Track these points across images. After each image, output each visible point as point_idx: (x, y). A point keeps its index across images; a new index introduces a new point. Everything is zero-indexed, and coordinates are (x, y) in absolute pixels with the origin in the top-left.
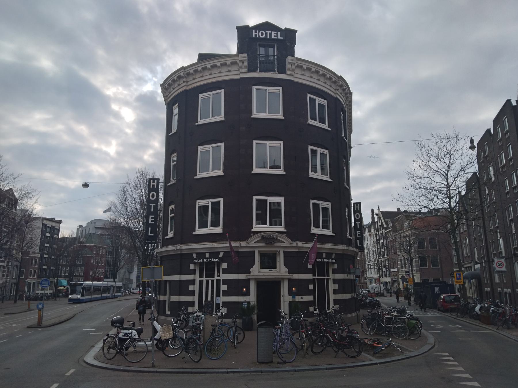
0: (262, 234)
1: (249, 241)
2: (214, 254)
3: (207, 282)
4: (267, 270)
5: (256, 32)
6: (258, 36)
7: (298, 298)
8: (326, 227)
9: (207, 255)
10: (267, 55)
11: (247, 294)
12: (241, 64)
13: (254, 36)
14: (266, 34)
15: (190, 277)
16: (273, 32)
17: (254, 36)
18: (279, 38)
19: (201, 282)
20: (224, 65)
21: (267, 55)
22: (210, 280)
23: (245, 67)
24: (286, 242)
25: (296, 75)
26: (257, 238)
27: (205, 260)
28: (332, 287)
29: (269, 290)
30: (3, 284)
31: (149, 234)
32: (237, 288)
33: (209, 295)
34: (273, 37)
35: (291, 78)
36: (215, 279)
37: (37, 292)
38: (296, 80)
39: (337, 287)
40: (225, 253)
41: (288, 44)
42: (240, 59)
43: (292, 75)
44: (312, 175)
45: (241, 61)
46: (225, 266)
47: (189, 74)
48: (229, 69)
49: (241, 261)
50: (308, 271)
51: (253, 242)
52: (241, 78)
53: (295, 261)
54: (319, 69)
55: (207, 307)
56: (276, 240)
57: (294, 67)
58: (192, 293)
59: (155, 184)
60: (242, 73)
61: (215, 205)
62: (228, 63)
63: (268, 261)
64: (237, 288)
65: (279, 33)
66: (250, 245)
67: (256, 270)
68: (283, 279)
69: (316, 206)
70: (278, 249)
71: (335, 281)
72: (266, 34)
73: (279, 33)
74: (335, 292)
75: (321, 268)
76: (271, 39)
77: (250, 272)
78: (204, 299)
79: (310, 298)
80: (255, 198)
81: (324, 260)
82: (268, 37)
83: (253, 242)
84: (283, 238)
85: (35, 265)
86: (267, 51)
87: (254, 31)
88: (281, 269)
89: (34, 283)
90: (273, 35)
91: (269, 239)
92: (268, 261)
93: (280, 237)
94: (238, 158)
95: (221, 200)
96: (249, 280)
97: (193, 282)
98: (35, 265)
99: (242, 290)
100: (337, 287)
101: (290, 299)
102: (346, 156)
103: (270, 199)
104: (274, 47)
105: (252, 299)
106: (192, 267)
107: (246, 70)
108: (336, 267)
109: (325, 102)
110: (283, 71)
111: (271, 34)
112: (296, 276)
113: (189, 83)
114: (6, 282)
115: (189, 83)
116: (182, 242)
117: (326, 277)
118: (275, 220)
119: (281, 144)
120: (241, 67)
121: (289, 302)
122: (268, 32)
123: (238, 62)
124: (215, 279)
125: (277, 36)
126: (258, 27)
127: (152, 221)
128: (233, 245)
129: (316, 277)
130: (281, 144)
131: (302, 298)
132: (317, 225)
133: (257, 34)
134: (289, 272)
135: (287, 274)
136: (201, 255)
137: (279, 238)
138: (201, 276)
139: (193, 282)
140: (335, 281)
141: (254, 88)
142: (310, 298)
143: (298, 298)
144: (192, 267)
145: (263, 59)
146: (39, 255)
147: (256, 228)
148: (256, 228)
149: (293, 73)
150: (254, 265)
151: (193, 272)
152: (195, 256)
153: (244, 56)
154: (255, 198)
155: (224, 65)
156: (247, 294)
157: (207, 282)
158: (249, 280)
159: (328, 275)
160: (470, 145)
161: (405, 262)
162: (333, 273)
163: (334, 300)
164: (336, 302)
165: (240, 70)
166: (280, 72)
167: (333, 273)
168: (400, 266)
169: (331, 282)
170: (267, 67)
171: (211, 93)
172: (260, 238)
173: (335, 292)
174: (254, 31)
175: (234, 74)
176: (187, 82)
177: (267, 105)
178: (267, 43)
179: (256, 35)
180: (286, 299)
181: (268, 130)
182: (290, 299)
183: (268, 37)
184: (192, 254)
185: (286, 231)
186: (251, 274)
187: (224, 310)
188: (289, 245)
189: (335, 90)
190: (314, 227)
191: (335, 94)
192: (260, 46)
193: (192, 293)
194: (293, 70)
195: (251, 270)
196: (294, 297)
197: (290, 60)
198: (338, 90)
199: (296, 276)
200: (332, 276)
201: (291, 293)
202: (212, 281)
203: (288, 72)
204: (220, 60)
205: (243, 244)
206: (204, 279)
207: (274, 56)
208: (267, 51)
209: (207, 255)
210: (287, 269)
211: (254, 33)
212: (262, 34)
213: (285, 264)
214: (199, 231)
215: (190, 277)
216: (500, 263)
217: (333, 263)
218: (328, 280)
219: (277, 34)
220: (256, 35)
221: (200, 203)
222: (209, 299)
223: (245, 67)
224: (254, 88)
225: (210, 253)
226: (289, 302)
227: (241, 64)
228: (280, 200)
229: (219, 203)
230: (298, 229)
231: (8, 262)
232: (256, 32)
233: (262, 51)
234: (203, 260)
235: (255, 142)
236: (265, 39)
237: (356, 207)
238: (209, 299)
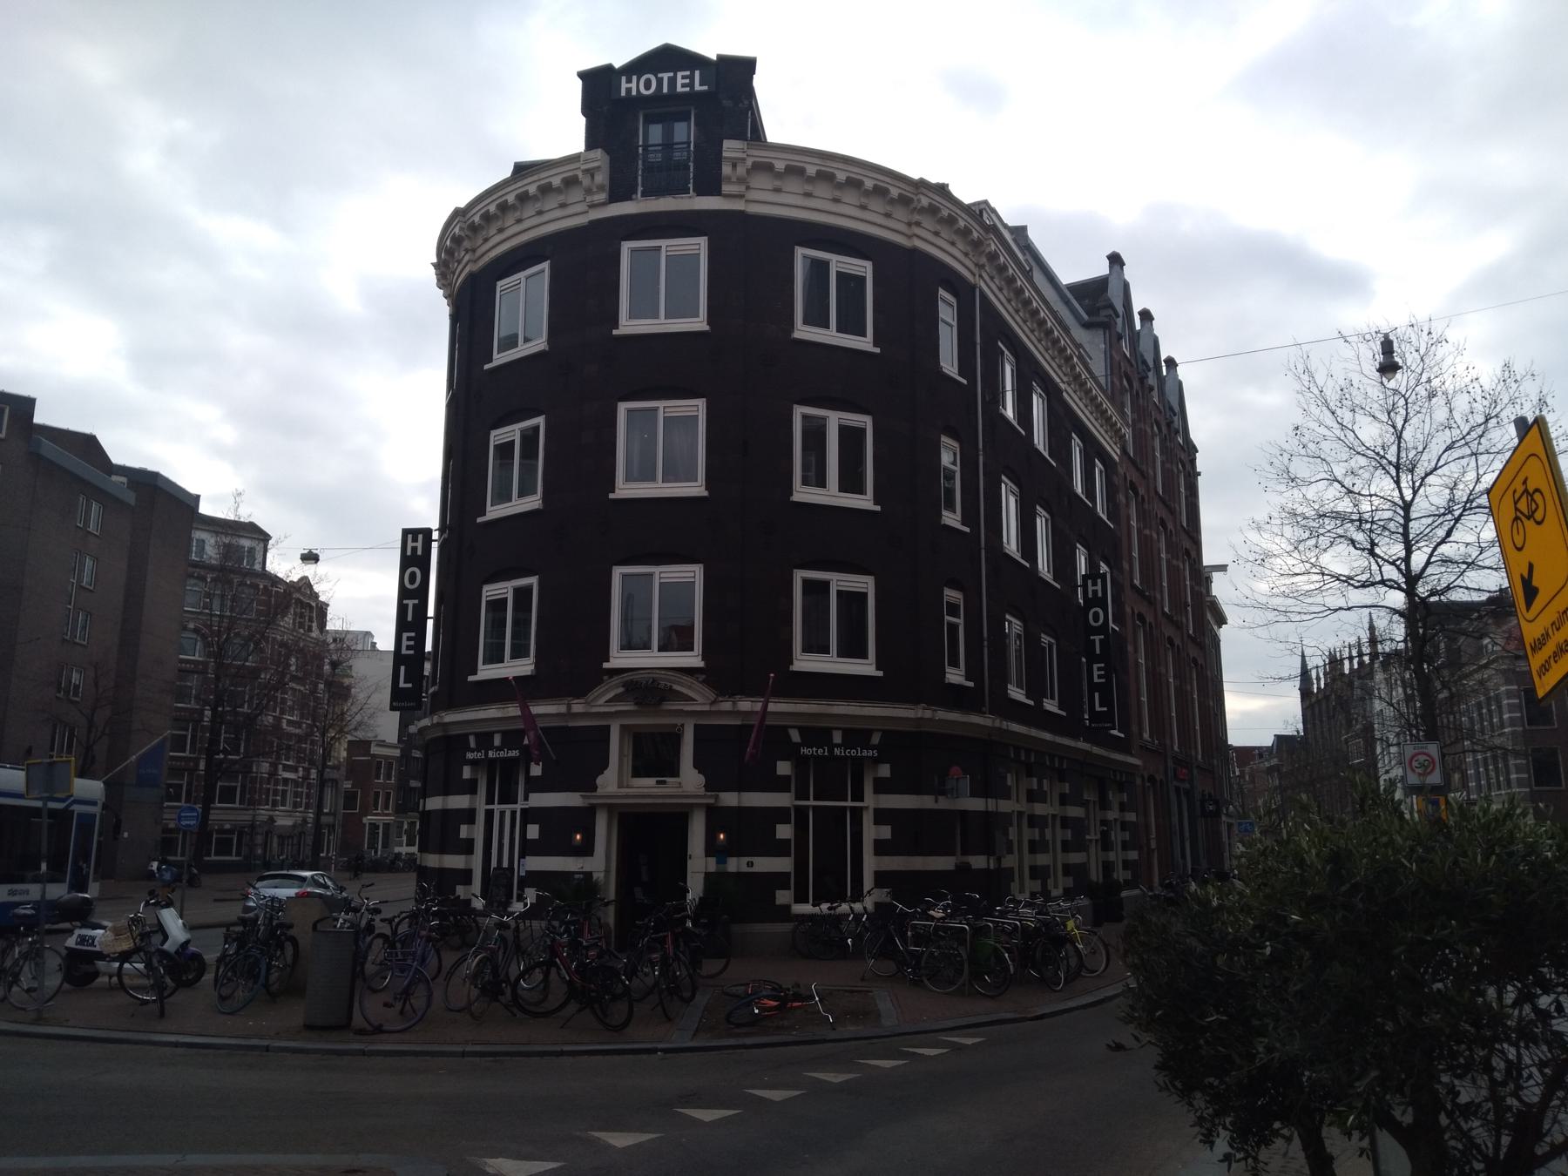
0: (627, 677)
1: (591, 696)
2: (857, 735)
3: (502, 813)
4: (651, 781)
5: (629, 81)
6: (634, 93)
7: (734, 865)
8: (851, 647)
9: (837, 738)
10: (668, 145)
11: (586, 850)
12: (586, 181)
13: (623, 93)
14: (660, 81)
15: (459, 802)
16: (679, 75)
17: (623, 93)
18: (697, 87)
19: (490, 814)
20: (546, 190)
21: (668, 145)
22: (508, 807)
23: (601, 188)
24: (700, 698)
25: (752, 195)
26: (613, 689)
27: (837, 751)
28: (872, 832)
29: (651, 837)
30: (294, 826)
31: (1098, 708)
32: (563, 832)
33: (502, 856)
34: (679, 89)
35: (738, 205)
36: (518, 807)
37: (397, 850)
38: (753, 209)
39: (886, 832)
40: (886, 734)
41: (727, 103)
42: (584, 167)
43: (741, 196)
44: (802, 494)
45: (586, 171)
46: (885, 771)
47: (474, 229)
48: (809, 188)
49: (575, 756)
50: (781, 785)
51: (601, 701)
52: (592, 223)
53: (729, 757)
54: (830, 167)
55: (499, 885)
56: (670, 694)
57: (741, 170)
58: (467, 847)
59: (419, 545)
60: (593, 206)
61: (522, 595)
62: (556, 181)
63: (654, 756)
64: (563, 832)
65: (697, 73)
66: (595, 710)
67: (609, 783)
68: (692, 805)
69: (816, 590)
70: (678, 721)
71: (881, 816)
72: (660, 81)
73: (697, 73)
74: (881, 848)
75: (832, 774)
76: (673, 96)
77: (595, 788)
78: (494, 864)
79: (783, 864)
80: (799, 576)
81: (831, 751)
82: (665, 90)
83: (601, 701)
84: (690, 687)
85: (388, 777)
86: (668, 134)
87: (624, 79)
88: (690, 780)
89: (387, 826)
90: (680, 81)
91: (647, 690)
92: (654, 756)
93: (679, 684)
94: (748, 454)
95: (533, 581)
96: (589, 813)
97: (469, 816)
98: (388, 777)
99: (571, 838)
100: (886, 832)
101: (712, 865)
102: (1547, 429)
103: (840, 582)
104: (687, 119)
105: (599, 863)
106: (467, 773)
107: (602, 197)
108: (885, 771)
109: (864, 268)
110: (710, 185)
111: (673, 81)
112: (730, 799)
113: (479, 252)
114: (305, 821)
115: (479, 252)
116: (451, 706)
117: (849, 804)
118: (677, 638)
119: (697, 408)
120: (589, 191)
121: (707, 875)
122: (666, 76)
123: (580, 175)
124: (518, 807)
125: (691, 85)
126: (640, 66)
127: (408, 648)
128: (536, 709)
129: (812, 803)
130: (697, 408)
131: (750, 864)
132: (816, 645)
133: (633, 86)
134: (708, 787)
135: (702, 791)
136: (816, 733)
137: (676, 687)
138: (490, 801)
139: (469, 816)
140: (881, 816)
141: (626, 247)
142: (783, 864)
143: (734, 865)
144: (784, 768)
145: (652, 158)
146: (397, 753)
147: (619, 659)
148: (619, 659)
149: (743, 188)
150: (606, 766)
151: (471, 788)
152: (795, 736)
153: (598, 153)
154: (799, 576)
155: (546, 190)
156: (586, 850)
157: (502, 813)
158: (589, 813)
159: (858, 796)
160: (1380, 358)
161: (1487, 770)
162: (877, 791)
163: (876, 873)
164: (881, 878)
165: (589, 199)
166: (701, 192)
167: (877, 791)
168: (1472, 784)
169: (868, 819)
170: (666, 180)
171: (522, 275)
172: (621, 690)
173: (881, 848)
174: (624, 79)
175: (574, 214)
176: (474, 251)
177: (666, 296)
178: (666, 108)
179: (629, 90)
180: (699, 865)
181: (663, 367)
182: (712, 865)
183: (665, 90)
184: (785, 728)
185: (702, 664)
186: (600, 791)
187: (531, 895)
188: (707, 708)
189: (909, 224)
190: (805, 650)
191: (910, 237)
192: (649, 120)
193: (467, 847)
194: (741, 181)
195: (600, 780)
196: (722, 861)
197: (734, 150)
198: (918, 224)
199: (730, 799)
200: (870, 800)
201: (711, 849)
202: (513, 813)
203: (726, 188)
204: (535, 178)
205: (578, 707)
206: (496, 807)
207: (689, 143)
208: (668, 134)
209: (837, 738)
210: (701, 779)
211: (624, 86)
212: (648, 85)
213: (697, 765)
214: (805, 663)
215: (459, 802)
216: (1422, 758)
217: (876, 761)
218: (857, 814)
219: (692, 77)
220: (629, 90)
221: (491, 591)
222: (505, 864)
223: (601, 188)
224: (626, 247)
225: (847, 733)
226: (707, 875)
227: (586, 181)
228: (864, 584)
229: (806, 582)
230: (909, 673)
231: (307, 770)
232: (629, 81)
233: (656, 133)
234: (831, 751)
235: (623, 407)
236: (658, 97)
237: (1090, 588)
238: (505, 864)
